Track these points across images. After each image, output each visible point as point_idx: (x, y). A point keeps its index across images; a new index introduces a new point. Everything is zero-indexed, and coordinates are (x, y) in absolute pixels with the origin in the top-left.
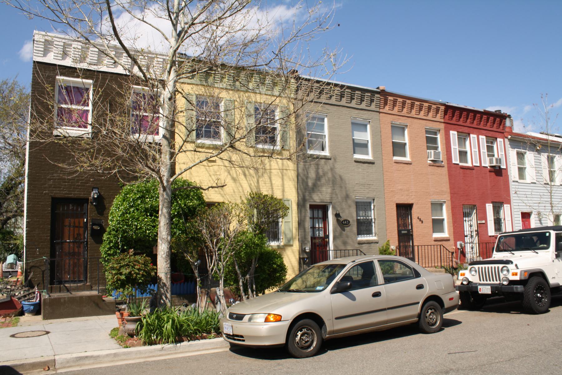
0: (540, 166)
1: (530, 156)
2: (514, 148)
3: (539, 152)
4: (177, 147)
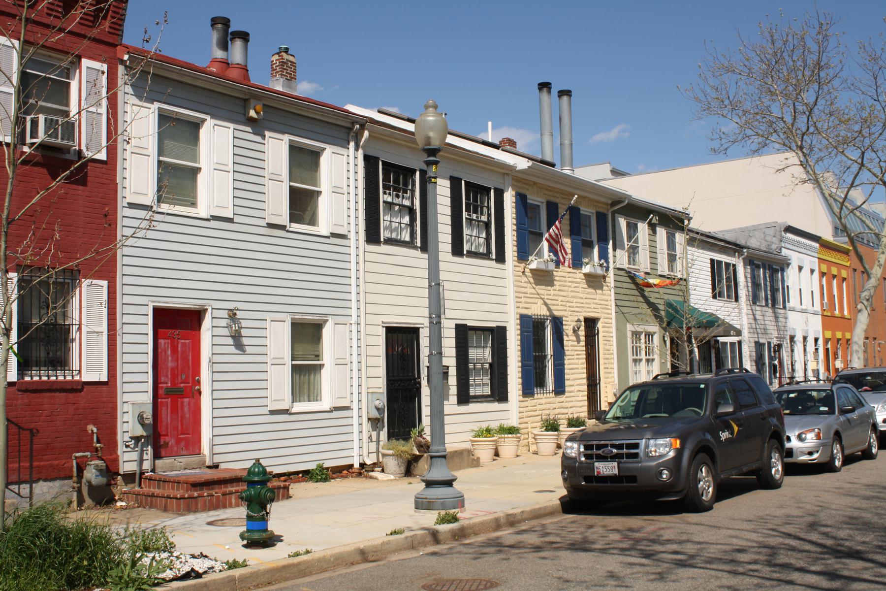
0: (619, 284)
1: (217, 139)
2: (152, 101)
3: (258, 127)
4: (119, 133)
